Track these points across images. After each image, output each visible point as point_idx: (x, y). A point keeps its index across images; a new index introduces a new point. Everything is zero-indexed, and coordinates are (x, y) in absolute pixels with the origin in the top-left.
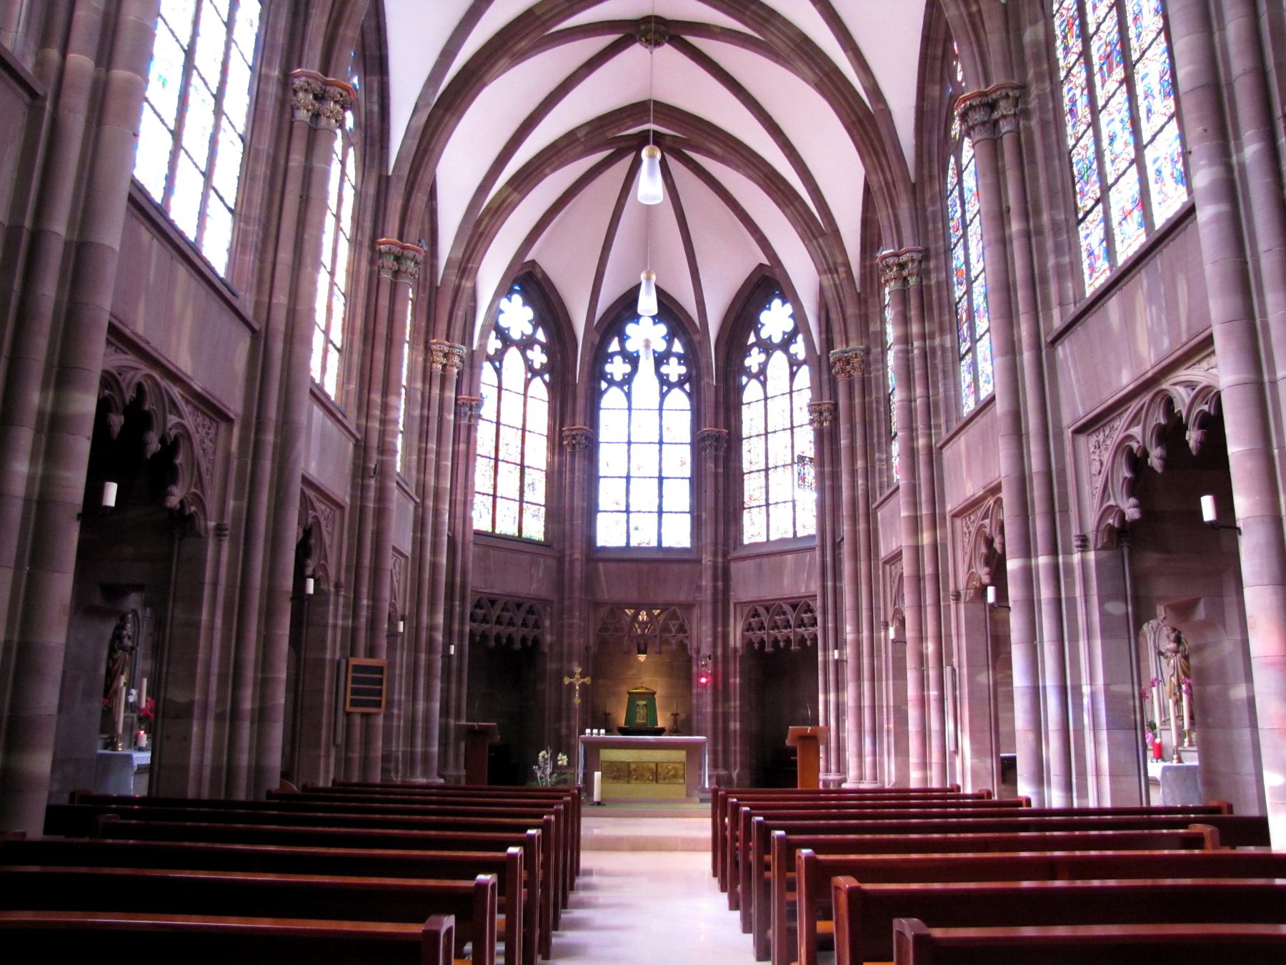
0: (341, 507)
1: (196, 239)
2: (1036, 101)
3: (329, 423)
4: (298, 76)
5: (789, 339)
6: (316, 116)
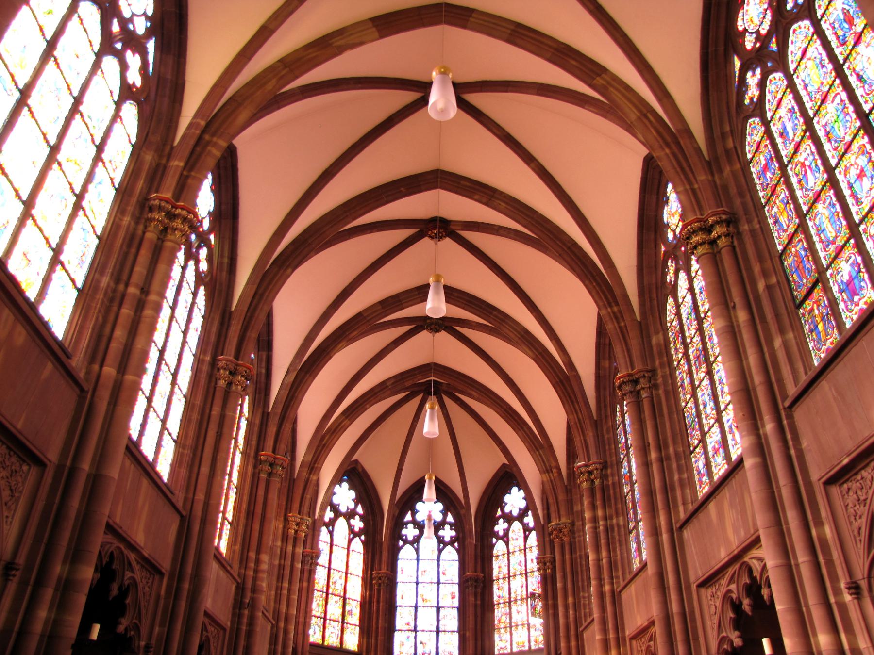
0: (224, 630)
1: (153, 460)
2: (661, 379)
3: (222, 573)
4: (221, 360)
5: (523, 514)
6: (230, 384)
